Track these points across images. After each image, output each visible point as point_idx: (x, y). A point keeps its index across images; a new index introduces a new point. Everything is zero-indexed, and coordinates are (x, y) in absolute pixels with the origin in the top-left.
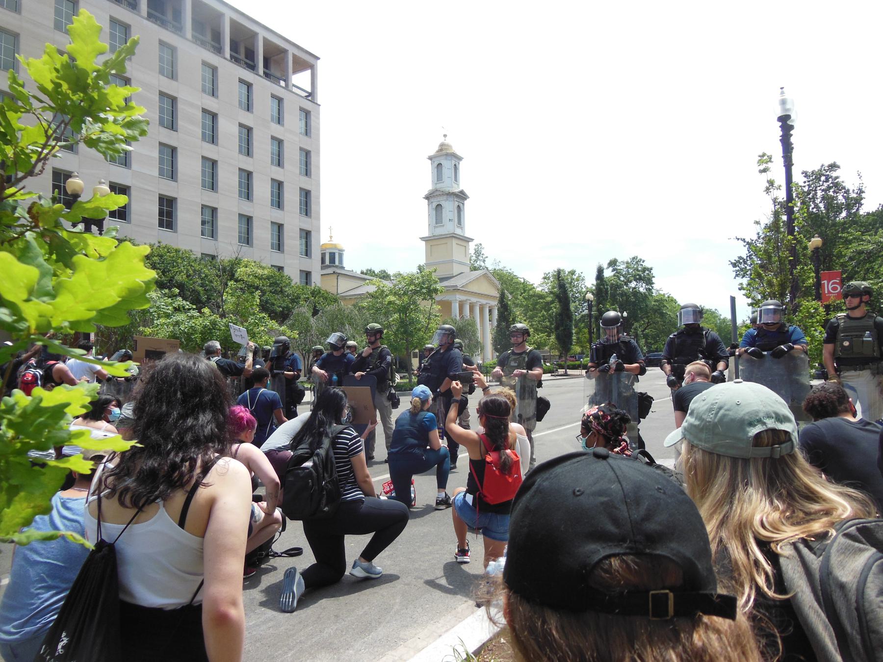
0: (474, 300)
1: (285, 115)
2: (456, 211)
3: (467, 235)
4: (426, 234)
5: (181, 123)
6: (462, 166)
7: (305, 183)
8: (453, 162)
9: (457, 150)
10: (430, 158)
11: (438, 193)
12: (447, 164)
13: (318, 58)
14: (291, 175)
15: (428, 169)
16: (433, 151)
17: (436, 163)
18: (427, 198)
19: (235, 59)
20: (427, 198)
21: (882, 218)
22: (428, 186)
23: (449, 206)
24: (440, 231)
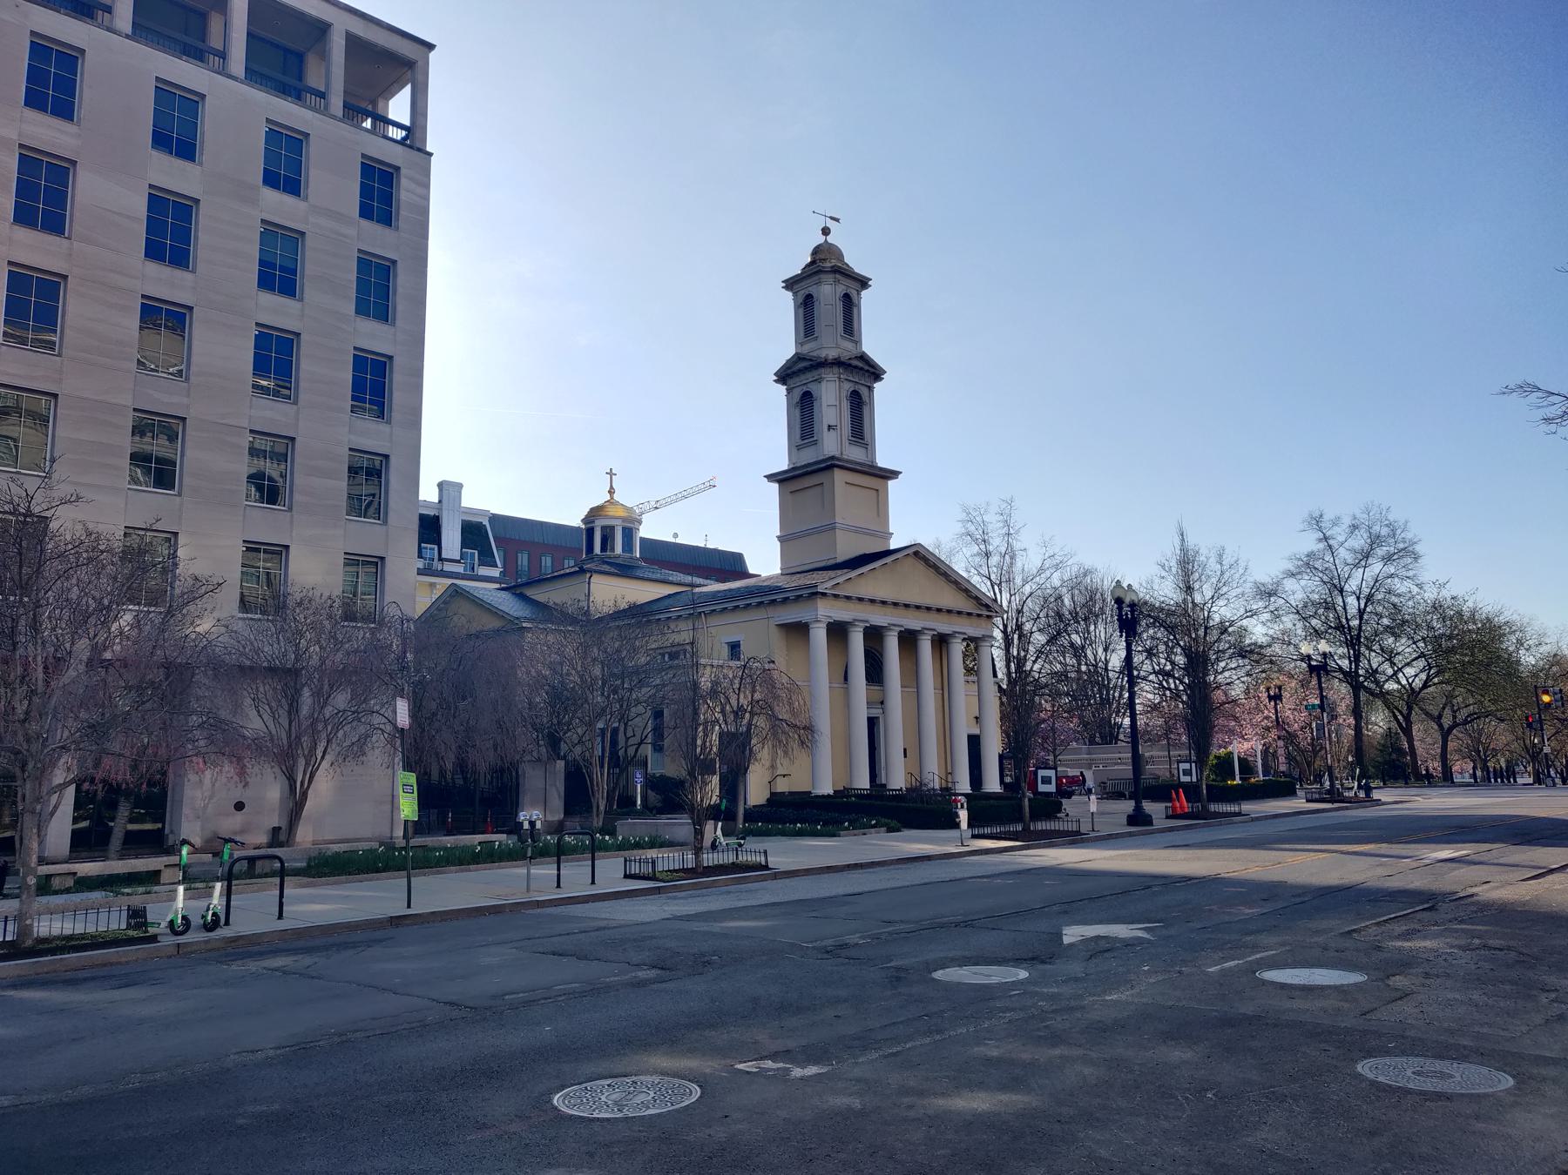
0: (879, 618)
1: (312, 172)
2: (846, 406)
3: (882, 461)
4: (782, 464)
5: (349, 275)
6: (868, 301)
7: (374, 336)
8: (841, 290)
9: (855, 260)
10: (790, 284)
11: (802, 365)
12: (828, 292)
13: (431, 47)
14: (326, 322)
15: (785, 305)
16: (798, 262)
17: (802, 294)
18: (784, 376)
19: (254, 75)
20: (784, 376)
21: (1563, 669)
22: (785, 348)
23: (831, 394)
24: (808, 456)
